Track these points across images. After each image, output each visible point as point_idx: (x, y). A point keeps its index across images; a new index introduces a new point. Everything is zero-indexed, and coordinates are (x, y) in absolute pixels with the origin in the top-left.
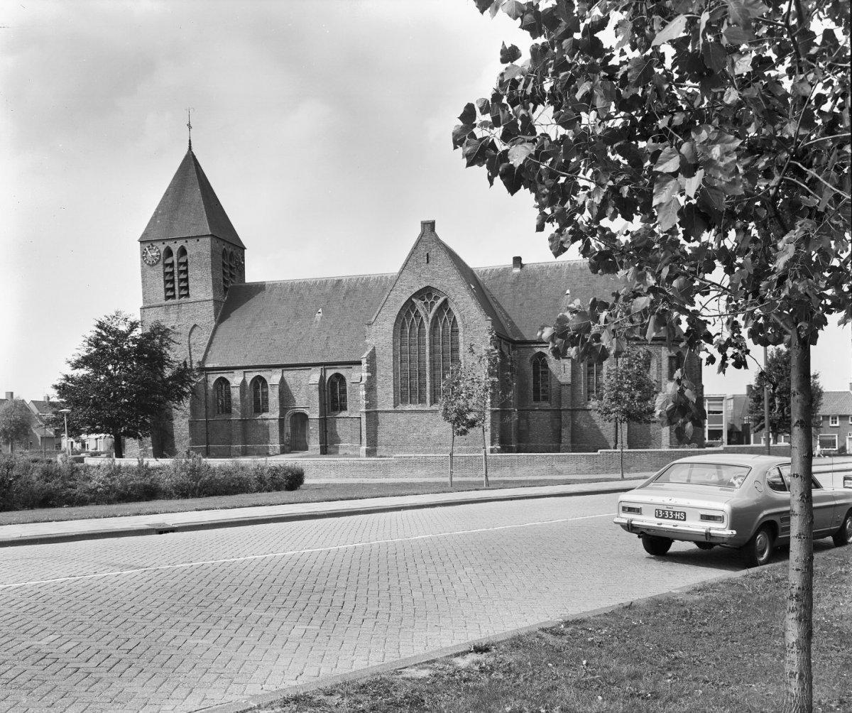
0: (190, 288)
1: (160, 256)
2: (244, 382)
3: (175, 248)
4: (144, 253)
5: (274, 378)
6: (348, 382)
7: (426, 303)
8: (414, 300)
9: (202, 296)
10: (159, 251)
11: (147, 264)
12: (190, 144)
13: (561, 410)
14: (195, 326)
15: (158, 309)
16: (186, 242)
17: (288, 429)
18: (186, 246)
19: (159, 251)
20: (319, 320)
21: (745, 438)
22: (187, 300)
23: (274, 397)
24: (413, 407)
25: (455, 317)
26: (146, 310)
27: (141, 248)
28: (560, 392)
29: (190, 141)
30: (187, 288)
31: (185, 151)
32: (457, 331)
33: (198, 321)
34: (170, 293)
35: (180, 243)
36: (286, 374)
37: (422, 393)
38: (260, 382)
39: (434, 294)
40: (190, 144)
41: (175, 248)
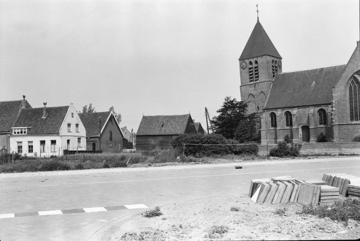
3: (253, 61)
5: (294, 112)
8: (355, 75)
9: (264, 80)
16: (257, 58)
27: (240, 62)
29: (258, 17)
31: (256, 22)
35: (255, 59)
38: (288, 115)
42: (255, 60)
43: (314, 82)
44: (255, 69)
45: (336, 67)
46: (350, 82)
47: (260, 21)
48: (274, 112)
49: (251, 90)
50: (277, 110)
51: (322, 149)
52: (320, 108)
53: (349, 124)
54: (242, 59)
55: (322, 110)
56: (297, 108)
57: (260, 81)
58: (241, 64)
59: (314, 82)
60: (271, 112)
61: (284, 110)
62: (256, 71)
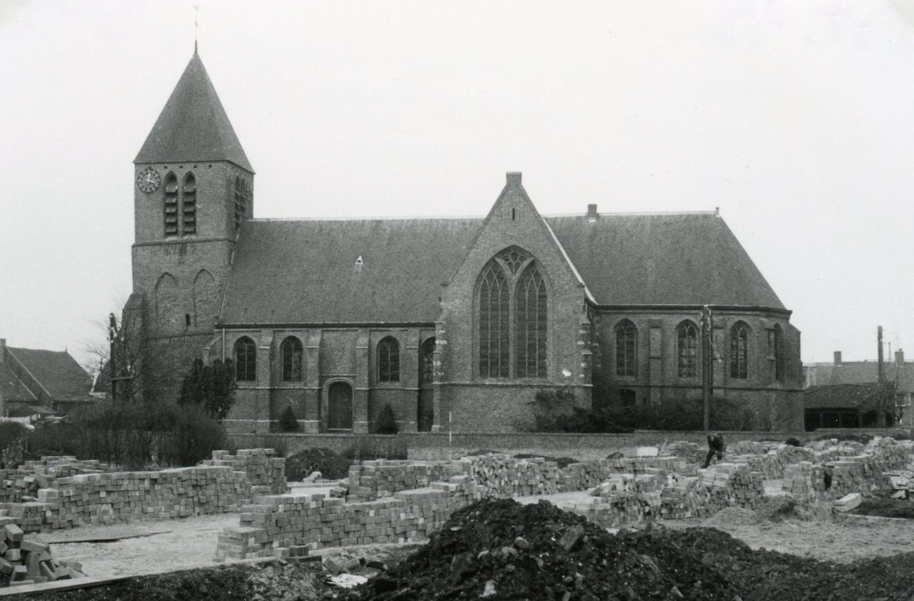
0: (198, 224)
1: (160, 182)
2: (273, 344)
3: (181, 174)
4: (139, 177)
5: (312, 340)
6: (402, 346)
7: (510, 264)
8: (498, 260)
9: (212, 234)
10: (159, 177)
11: (143, 191)
12: (196, 45)
13: (650, 387)
14: (203, 270)
15: (157, 248)
16: (210, 166)
17: (326, 401)
18: (194, 173)
19: (159, 177)
20: (360, 270)
21: (119, 325)
22: (193, 237)
23: (311, 362)
24: (494, 381)
25: (543, 281)
26: (140, 249)
27: (136, 171)
28: (649, 365)
29: (196, 42)
30: (193, 223)
31: (190, 56)
32: (545, 297)
33: (207, 265)
34: (171, 227)
35: (188, 168)
36: (326, 335)
37: (505, 363)
38: (292, 346)
39: (520, 254)
40: (196, 45)
41: (181, 174)
42: (186, 171)
43: (360, 258)
44: (186, 200)
45: (415, 221)
46: (485, 275)
47: (199, 53)
48: (250, 335)
49: (167, 262)
50: (260, 331)
51: (441, 450)
52: (385, 334)
53: (477, 386)
54: (144, 162)
55: (389, 340)
56: (319, 331)
57: (201, 237)
58: (139, 178)
59: (360, 258)
60: (242, 335)
61: (281, 334)
62: (187, 204)
